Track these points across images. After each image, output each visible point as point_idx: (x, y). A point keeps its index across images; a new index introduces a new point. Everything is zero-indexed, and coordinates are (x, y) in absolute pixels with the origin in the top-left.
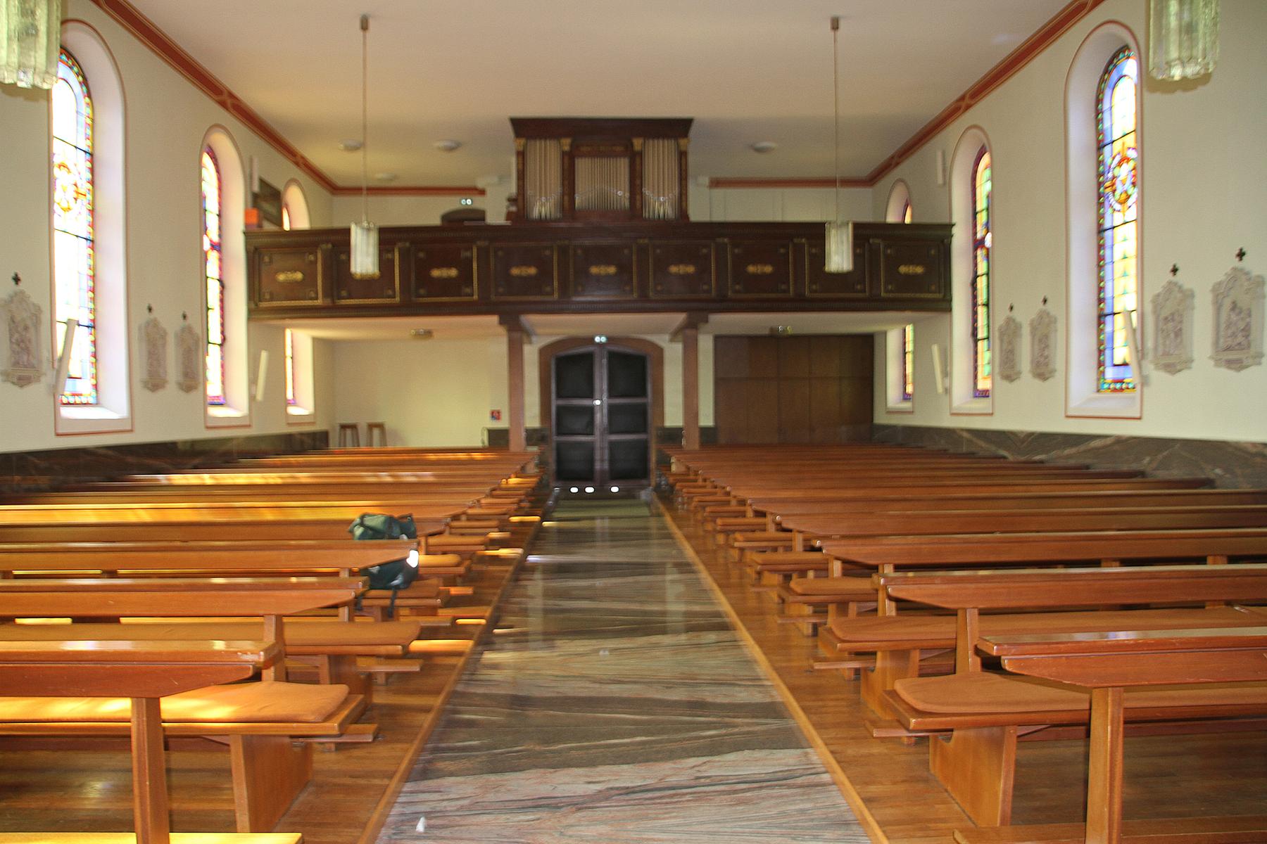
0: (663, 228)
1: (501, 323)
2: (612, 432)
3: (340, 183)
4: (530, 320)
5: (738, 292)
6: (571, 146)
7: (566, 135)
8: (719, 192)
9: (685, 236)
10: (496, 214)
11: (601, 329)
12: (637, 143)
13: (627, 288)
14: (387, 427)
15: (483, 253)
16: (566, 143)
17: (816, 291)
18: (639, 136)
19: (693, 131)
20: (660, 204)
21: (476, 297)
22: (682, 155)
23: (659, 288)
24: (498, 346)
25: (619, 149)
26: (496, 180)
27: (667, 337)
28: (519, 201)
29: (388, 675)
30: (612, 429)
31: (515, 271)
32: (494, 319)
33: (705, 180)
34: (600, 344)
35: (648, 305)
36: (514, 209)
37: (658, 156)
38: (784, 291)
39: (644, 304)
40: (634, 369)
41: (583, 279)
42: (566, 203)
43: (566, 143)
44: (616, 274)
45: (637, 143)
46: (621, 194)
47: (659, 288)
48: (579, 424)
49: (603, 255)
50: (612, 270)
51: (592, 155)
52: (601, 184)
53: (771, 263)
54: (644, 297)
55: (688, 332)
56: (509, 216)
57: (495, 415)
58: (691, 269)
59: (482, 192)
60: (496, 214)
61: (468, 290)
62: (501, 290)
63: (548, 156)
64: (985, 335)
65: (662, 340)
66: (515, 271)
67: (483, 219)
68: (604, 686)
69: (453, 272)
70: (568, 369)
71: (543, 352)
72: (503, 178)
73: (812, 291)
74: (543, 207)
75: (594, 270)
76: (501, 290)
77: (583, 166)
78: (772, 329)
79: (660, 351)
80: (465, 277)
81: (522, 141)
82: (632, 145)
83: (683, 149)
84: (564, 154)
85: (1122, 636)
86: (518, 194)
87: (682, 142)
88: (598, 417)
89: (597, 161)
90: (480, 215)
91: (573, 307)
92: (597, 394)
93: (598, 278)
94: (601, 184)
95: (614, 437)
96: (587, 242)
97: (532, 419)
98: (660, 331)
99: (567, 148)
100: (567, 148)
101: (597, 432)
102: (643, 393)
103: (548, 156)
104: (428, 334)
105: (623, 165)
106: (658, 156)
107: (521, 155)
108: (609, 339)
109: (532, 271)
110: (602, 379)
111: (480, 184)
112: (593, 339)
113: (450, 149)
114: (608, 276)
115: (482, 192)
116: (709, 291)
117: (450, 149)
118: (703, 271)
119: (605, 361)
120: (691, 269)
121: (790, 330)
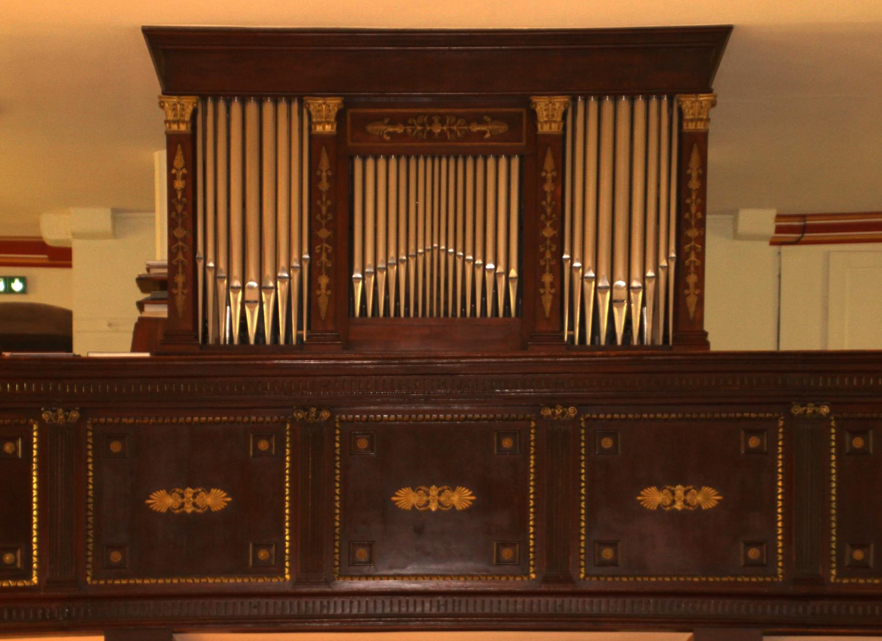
0: (622, 365)
5: (859, 568)
6: (340, 117)
7: (325, 90)
8: (803, 259)
10: (105, 324)
12: (548, 110)
13: (507, 554)
15: (62, 448)
16: (325, 111)
18: (551, 90)
20: (615, 293)
21: (35, 579)
22: (690, 147)
23: (608, 553)
26: (101, 219)
28: (177, 285)
29: (569, 330)
31: (162, 501)
33: (761, 220)
35: (573, 605)
36: (160, 311)
37: (613, 155)
41: (373, 526)
43: (325, 111)
45: (548, 110)
46: (493, 270)
47: (608, 553)
49: (435, 455)
50: (461, 498)
51: (402, 150)
52: (434, 239)
54: (558, 578)
56: (144, 333)
58: (707, 498)
59: (61, 257)
60: (105, 324)
62: (116, 557)
63: (266, 156)
64: (384, 266)
66: (162, 501)
67: (67, 343)
68: (547, 589)
72: (122, 218)
74: (252, 304)
75: (407, 498)
76: (116, 557)
77: (377, 183)
81: (188, 103)
82: (533, 115)
84: (316, 142)
86: (172, 266)
87: (690, 104)
89: (422, 167)
90: (56, 327)
91: (338, 607)
93: (419, 522)
94: (434, 239)
105: (502, 179)
107: (183, 147)
109: (215, 499)
111: (53, 231)
114: (449, 514)
115: (61, 257)
116: (763, 566)
118: (746, 503)
120: (707, 498)
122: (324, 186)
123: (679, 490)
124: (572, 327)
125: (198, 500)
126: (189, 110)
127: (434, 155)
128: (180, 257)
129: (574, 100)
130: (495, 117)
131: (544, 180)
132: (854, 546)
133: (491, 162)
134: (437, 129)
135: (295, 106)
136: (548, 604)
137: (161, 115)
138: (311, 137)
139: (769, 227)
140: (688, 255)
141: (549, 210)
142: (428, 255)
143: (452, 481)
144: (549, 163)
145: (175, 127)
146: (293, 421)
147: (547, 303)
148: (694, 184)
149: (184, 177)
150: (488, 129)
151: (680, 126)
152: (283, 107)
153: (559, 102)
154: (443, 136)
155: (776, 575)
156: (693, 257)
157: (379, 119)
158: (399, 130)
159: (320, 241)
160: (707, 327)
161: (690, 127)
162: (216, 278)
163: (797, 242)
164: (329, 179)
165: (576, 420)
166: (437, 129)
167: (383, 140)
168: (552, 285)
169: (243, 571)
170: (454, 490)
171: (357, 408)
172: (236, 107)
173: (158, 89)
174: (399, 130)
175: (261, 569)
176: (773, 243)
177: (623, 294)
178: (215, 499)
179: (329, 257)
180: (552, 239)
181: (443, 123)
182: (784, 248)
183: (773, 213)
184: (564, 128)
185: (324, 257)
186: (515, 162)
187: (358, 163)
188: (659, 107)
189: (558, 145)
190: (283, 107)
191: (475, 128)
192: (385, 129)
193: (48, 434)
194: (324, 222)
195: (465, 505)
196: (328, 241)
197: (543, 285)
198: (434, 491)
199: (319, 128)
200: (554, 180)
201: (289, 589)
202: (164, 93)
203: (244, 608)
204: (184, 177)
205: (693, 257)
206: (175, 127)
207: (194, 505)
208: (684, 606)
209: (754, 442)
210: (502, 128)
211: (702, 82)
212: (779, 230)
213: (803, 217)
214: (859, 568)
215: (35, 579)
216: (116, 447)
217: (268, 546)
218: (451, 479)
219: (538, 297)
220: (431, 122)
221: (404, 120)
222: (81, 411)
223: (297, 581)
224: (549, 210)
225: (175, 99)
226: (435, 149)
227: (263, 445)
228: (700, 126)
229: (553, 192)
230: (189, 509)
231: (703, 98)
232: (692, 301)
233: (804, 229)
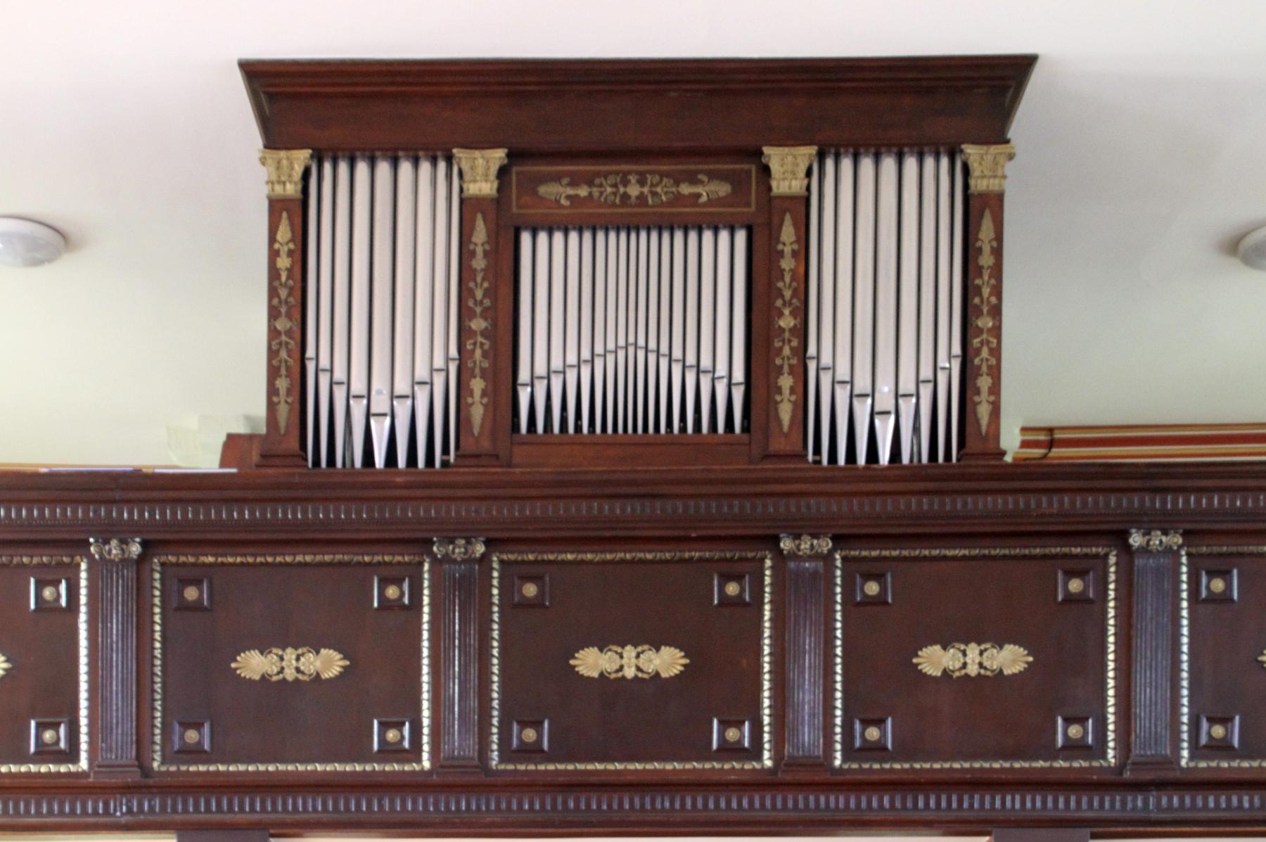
12: (787, 167)
16: (482, 170)
17: (194, 753)
19: (1026, 121)
21: (84, 764)
22: (979, 213)
25: (710, 190)
38: (390, 752)
52: (625, 324)
61: (57, 736)
73: (507, 754)
77: (550, 261)
83: (979, 185)
84: (469, 207)
85: (570, 557)
89: (613, 244)
94: (625, 324)
99: (484, 187)
100: (484, 187)
103: (402, 228)
105: (722, 257)
106: (874, 227)
107: (293, 214)
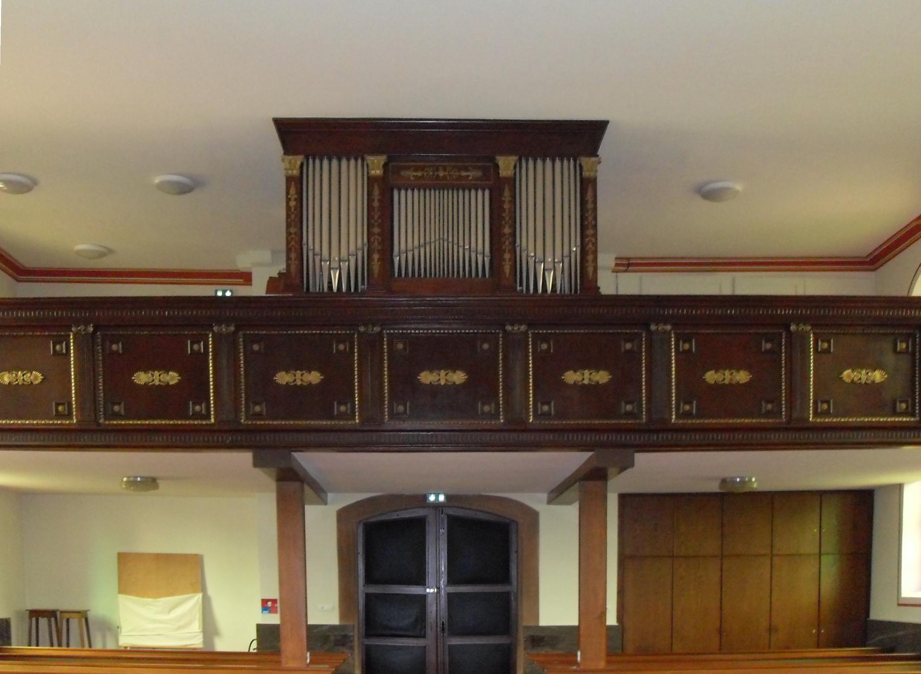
0: (550, 311)
1: (258, 463)
2: (454, 633)
3: (27, 262)
4: (311, 461)
6: (385, 166)
7: (375, 151)
9: (591, 321)
11: (437, 475)
12: (506, 164)
14: (90, 615)
15: (226, 345)
16: (376, 164)
20: (547, 267)
22: (587, 186)
24: (261, 505)
27: (544, 496)
30: (453, 627)
32: (245, 457)
34: (437, 506)
37: (543, 188)
39: (516, 437)
40: (492, 545)
42: (376, 267)
43: (376, 164)
44: (463, 385)
45: (506, 164)
46: (475, 245)
48: (405, 618)
49: (442, 353)
52: (439, 231)
53: (748, 368)
55: (590, 484)
57: (267, 605)
58: (602, 377)
63: (342, 190)
65: (536, 501)
69: (172, 378)
70: (383, 543)
71: (344, 515)
77: (406, 203)
78: (724, 481)
79: (533, 517)
80: (194, 383)
81: (299, 159)
82: (497, 167)
84: (371, 180)
87: (586, 161)
88: (431, 609)
89: (432, 197)
92: (430, 578)
94: (439, 231)
95: (456, 641)
96: (416, 329)
97: (324, 607)
98: (530, 487)
99: (378, 172)
101: (430, 633)
102: (505, 579)
103: (342, 190)
104: (150, 483)
105: (480, 201)
106: (543, 188)
107: (296, 184)
108: (448, 497)
109: (314, 377)
110: (438, 559)
112: (425, 497)
113: (183, 189)
117: (183, 189)
119: (443, 531)
120: (602, 377)
121: (755, 484)
122: (376, 204)
123: (587, 372)
124: (521, 285)
125: (304, 378)
126: (299, 163)
127: (442, 188)
128: (293, 243)
129: (520, 160)
130: (475, 168)
131: (504, 202)
132: (543, 404)
133: (473, 192)
134: (441, 174)
135: (360, 161)
136: (513, 437)
137: (283, 166)
138: (368, 178)
139: (612, 263)
140: (587, 244)
141: (507, 219)
142: (437, 243)
143: (453, 367)
144: (507, 193)
145: (290, 172)
146: (359, 333)
147: (507, 268)
148: (590, 206)
149: (296, 199)
150: (472, 174)
151: (581, 174)
152: (352, 162)
153: (513, 159)
154: (444, 178)
155: (642, 418)
156: (590, 246)
157: (408, 168)
158: (419, 174)
159: (374, 234)
160: (599, 284)
161: (586, 174)
162: (314, 255)
163: (626, 271)
164: (379, 200)
165: (525, 334)
166: (441, 174)
167: (409, 179)
168: (510, 260)
169: (332, 418)
170: (454, 372)
171: (401, 326)
172: (326, 162)
173: (282, 152)
174: (419, 174)
175: (341, 416)
176: (613, 271)
177: (551, 266)
178: (314, 377)
179: (379, 244)
180: (510, 234)
181: (445, 170)
182: (619, 274)
183: (614, 256)
184: (515, 174)
185: (376, 243)
186: (487, 193)
187: (396, 193)
188: (568, 166)
189: (512, 182)
190: (352, 162)
191: (464, 174)
192: (411, 174)
193: (218, 338)
194: (376, 224)
195: (462, 381)
196: (379, 234)
197: (504, 260)
198: (443, 373)
199: (373, 172)
200: (510, 202)
201: (358, 428)
202: (285, 154)
203: (332, 438)
204: (296, 199)
205: (590, 246)
206: (290, 172)
207: (302, 380)
208: (589, 438)
209: (628, 346)
210: (479, 174)
211: (593, 151)
212: (617, 265)
213: (628, 259)
214: (688, 415)
215: (213, 420)
216: (256, 347)
217: (346, 404)
218: (453, 366)
219: (501, 267)
220: (437, 170)
221: (422, 169)
222: (236, 326)
223: (362, 422)
224: (507, 219)
225: (290, 157)
226: (439, 185)
227: (341, 347)
228: (592, 174)
229: (509, 209)
230: (299, 383)
231: (593, 159)
232: (590, 270)
233: (629, 265)
